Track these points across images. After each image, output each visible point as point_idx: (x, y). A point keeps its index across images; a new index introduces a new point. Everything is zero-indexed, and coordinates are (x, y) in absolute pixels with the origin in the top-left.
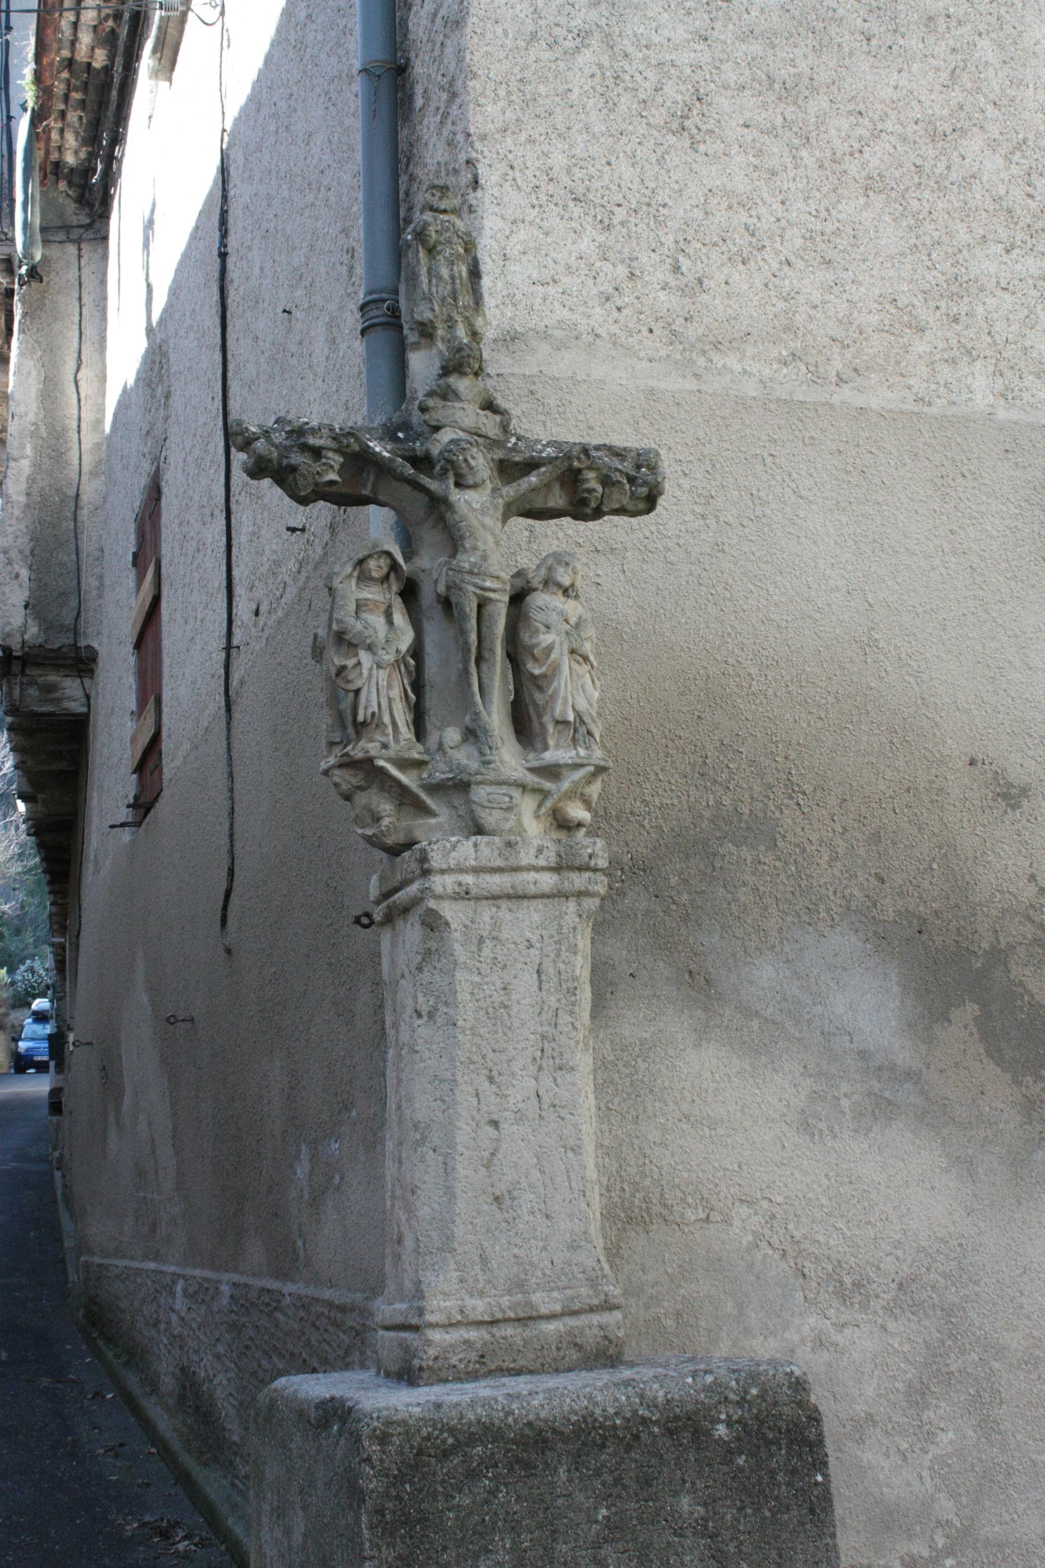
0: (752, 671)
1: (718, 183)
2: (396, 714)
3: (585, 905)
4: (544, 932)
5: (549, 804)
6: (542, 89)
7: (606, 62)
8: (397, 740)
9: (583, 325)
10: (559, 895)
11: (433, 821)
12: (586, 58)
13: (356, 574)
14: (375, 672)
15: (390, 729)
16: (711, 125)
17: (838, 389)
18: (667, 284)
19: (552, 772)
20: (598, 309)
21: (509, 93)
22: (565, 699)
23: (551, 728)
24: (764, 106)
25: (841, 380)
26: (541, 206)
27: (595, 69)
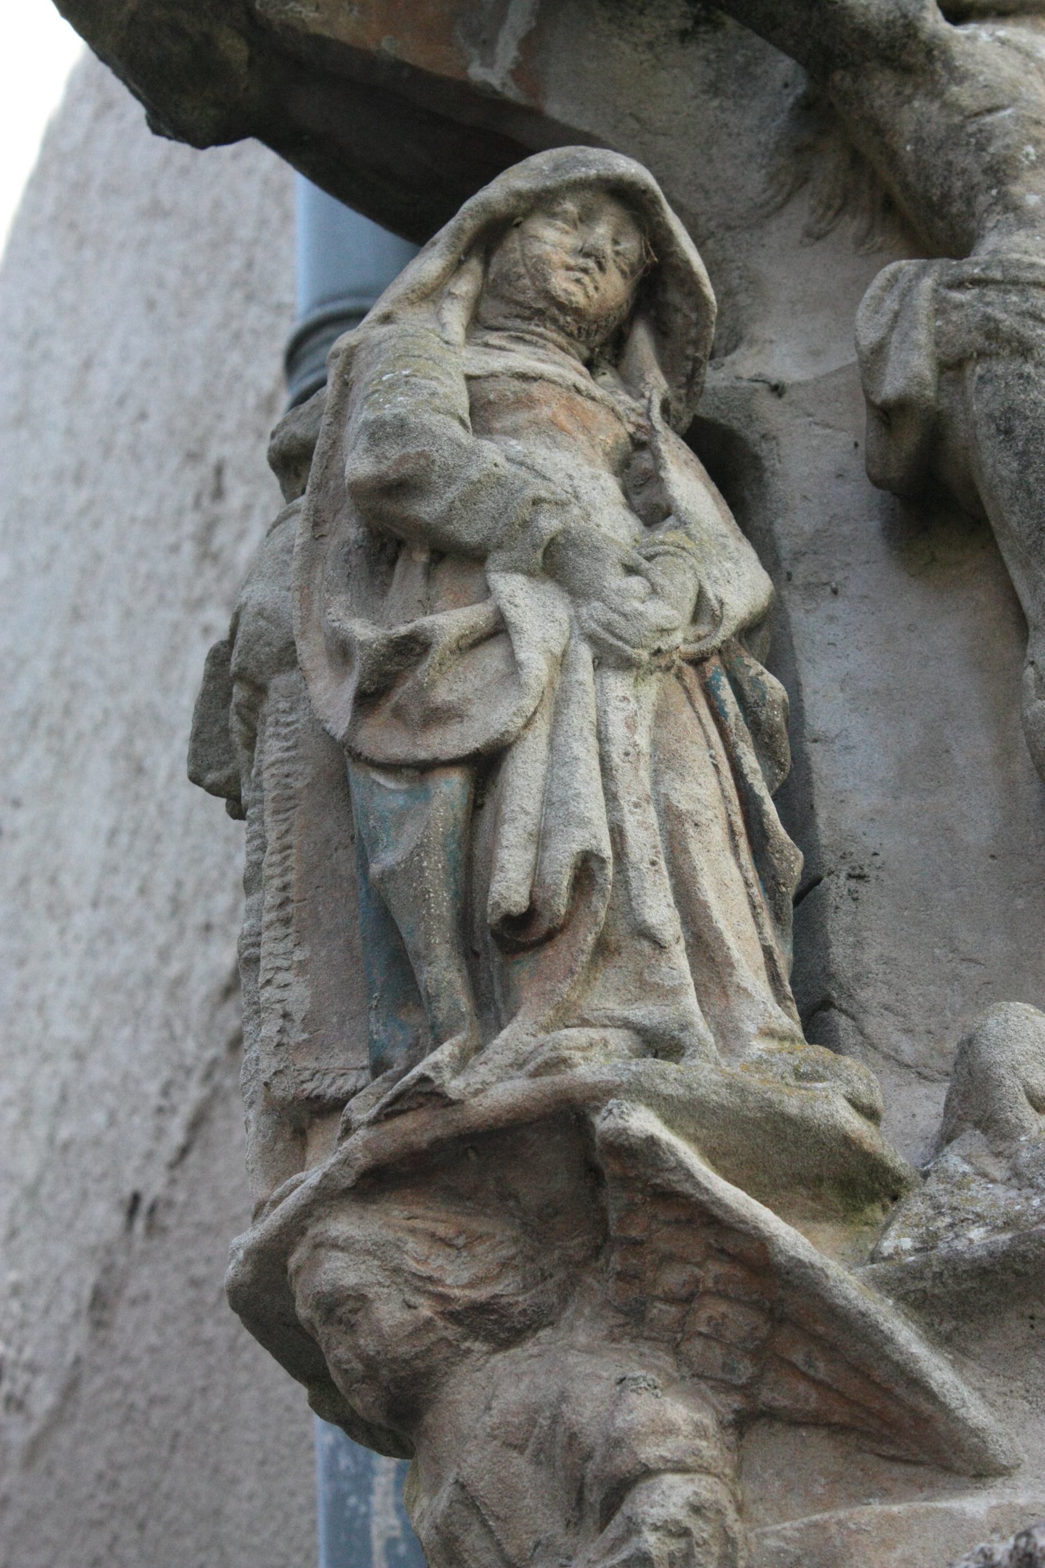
13: (465, 286)
15: (680, 960)
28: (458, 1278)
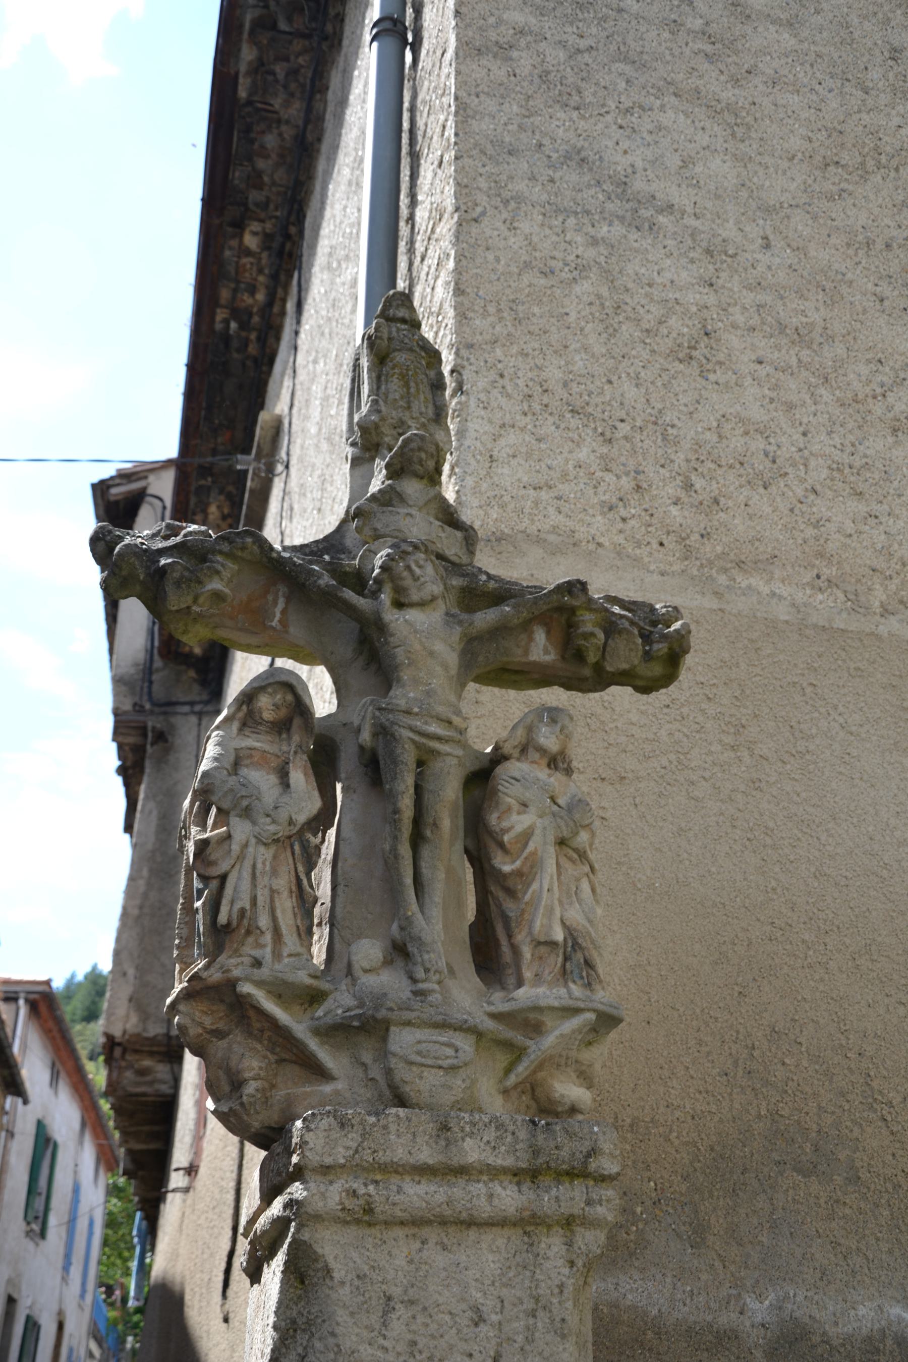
0: (807, 937)
1: (732, 410)
2: (279, 914)
3: (579, 1242)
4: (505, 1292)
5: (522, 1069)
6: (536, 310)
7: (604, 291)
8: (277, 955)
9: (582, 533)
10: (529, 1223)
11: (328, 1088)
12: (584, 287)
13: (241, 715)
14: (251, 849)
15: (268, 938)
16: (721, 357)
17: (883, 620)
18: (679, 499)
19: (529, 1022)
20: (599, 518)
21: (499, 311)
22: (550, 911)
23: (527, 952)
24: (778, 347)
25: (886, 612)
26: (534, 414)
27: (592, 298)
28: (208, 1021)
